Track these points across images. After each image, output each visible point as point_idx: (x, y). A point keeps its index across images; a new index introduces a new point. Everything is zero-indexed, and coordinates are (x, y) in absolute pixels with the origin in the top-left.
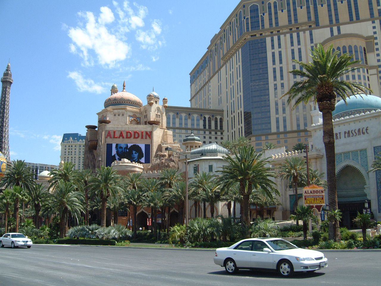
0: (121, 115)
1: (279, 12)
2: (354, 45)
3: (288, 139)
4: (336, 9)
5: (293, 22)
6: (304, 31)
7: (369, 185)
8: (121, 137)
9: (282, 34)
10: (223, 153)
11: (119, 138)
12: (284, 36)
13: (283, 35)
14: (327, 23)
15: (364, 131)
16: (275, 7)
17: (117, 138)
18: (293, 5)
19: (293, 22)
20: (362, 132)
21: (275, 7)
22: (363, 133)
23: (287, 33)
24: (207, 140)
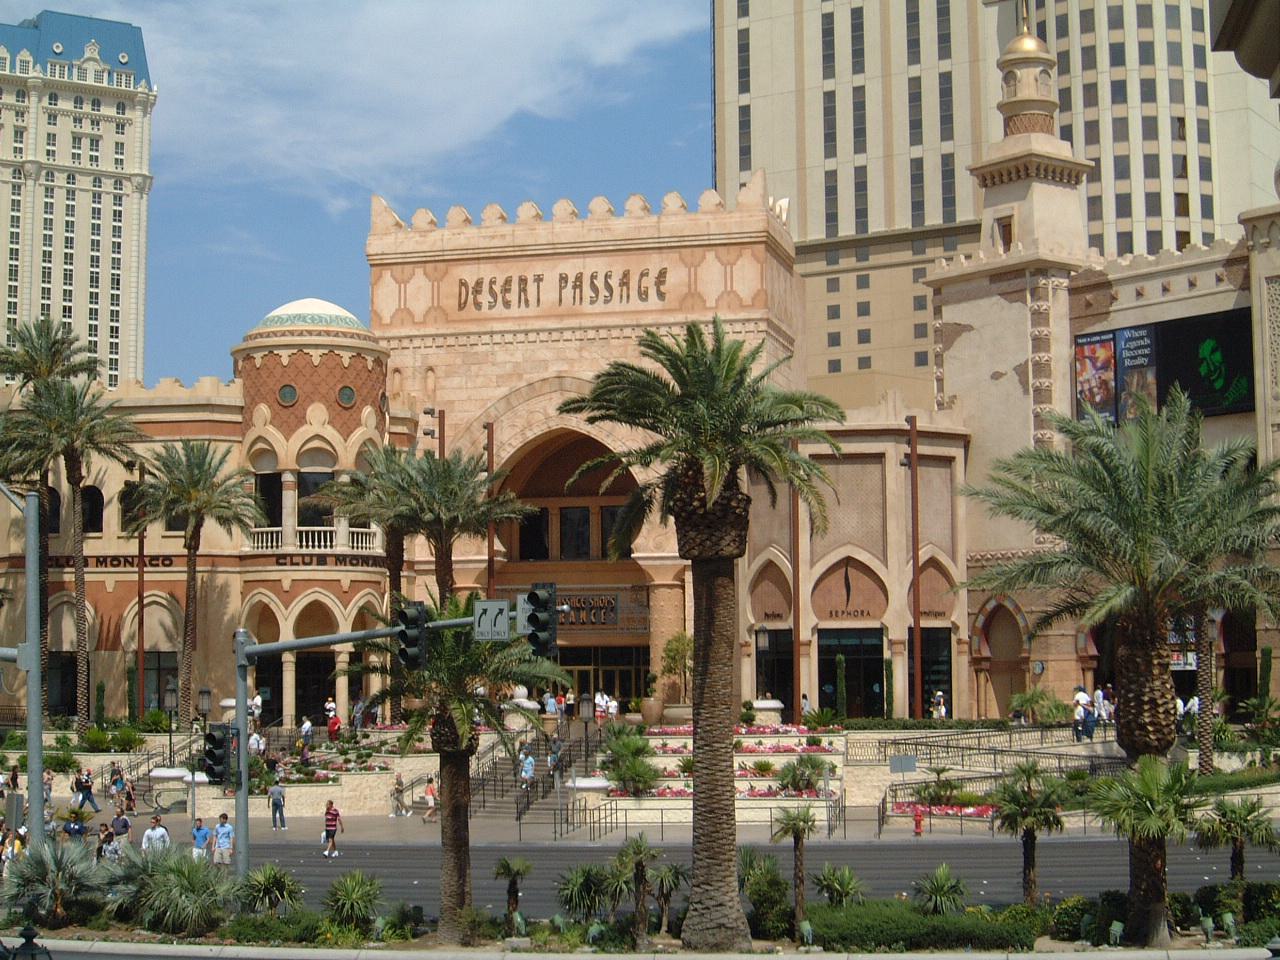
0: (111, 673)
3: (871, 273)
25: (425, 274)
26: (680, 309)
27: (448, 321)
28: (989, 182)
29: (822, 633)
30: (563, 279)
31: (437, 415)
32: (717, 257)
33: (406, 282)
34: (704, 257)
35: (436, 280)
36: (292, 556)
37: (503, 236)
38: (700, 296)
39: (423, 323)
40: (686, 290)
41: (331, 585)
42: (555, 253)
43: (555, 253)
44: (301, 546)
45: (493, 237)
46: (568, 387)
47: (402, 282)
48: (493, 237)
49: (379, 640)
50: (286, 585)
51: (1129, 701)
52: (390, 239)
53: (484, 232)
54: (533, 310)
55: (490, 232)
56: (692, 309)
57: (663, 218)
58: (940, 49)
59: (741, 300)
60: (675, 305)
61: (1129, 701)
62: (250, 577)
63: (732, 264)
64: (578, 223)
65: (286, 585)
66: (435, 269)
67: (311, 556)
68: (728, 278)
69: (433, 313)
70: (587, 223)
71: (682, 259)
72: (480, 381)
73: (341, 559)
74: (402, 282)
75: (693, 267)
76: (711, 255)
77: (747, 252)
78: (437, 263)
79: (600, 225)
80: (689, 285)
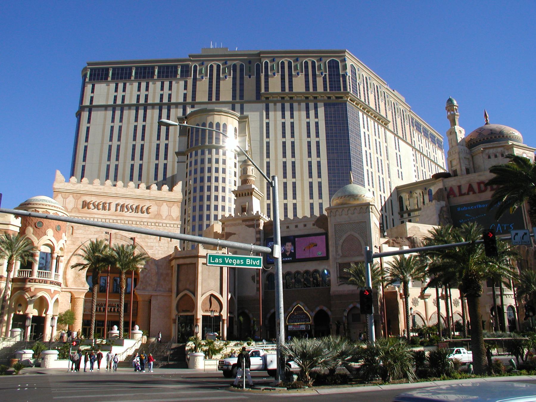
1: (246, 77)
2: (223, 123)
4: (242, 84)
5: (287, 90)
6: (299, 102)
7: (39, 272)
8: (471, 193)
9: (272, 102)
10: (46, 265)
11: (468, 194)
12: (274, 105)
13: (297, 104)
14: (230, 99)
15: (144, 209)
16: (242, 70)
17: (464, 194)
18: (240, 71)
19: (287, 90)
20: (141, 211)
21: (242, 70)
22: (142, 212)
23: (278, 101)
24: (189, 228)
25: (73, 197)
26: (154, 218)
27: (79, 212)
28: (238, 196)
29: (203, 316)
30: (117, 205)
31: (378, 248)
32: (167, 204)
33: (66, 198)
34: (163, 204)
35: (77, 199)
36: (35, 280)
37: (101, 189)
38: (161, 215)
39: (71, 212)
40: (156, 213)
41: (48, 291)
42: (116, 197)
43: (116, 197)
44: (39, 277)
45: (97, 189)
46: (118, 237)
47: (65, 198)
48: (97, 189)
49: (428, 389)
50: (52, 292)
51: (360, 354)
52: (62, 184)
53: (95, 187)
54: (106, 212)
55: (96, 187)
56: (158, 219)
57: (151, 191)
58: (158, 166)
59: (173, 218)
60: (153, 217)
61: (360, 354)
62: (226, 322)
63: (171, 207)
64: (125, 188)
65: (52, 292)
66: (77, 196)
67: (42, 280)
68: (169, 211)
69: (75, 209)
70: (128, 189)
71: (156, 204)
72: (88, 232)
73: (52, 283)
74: (65, 198)
75: (159, 206)
76: (165, 204)
77: (176, 204)
78: (77, 194)
79: (132, 190)
80: (158, 212)
